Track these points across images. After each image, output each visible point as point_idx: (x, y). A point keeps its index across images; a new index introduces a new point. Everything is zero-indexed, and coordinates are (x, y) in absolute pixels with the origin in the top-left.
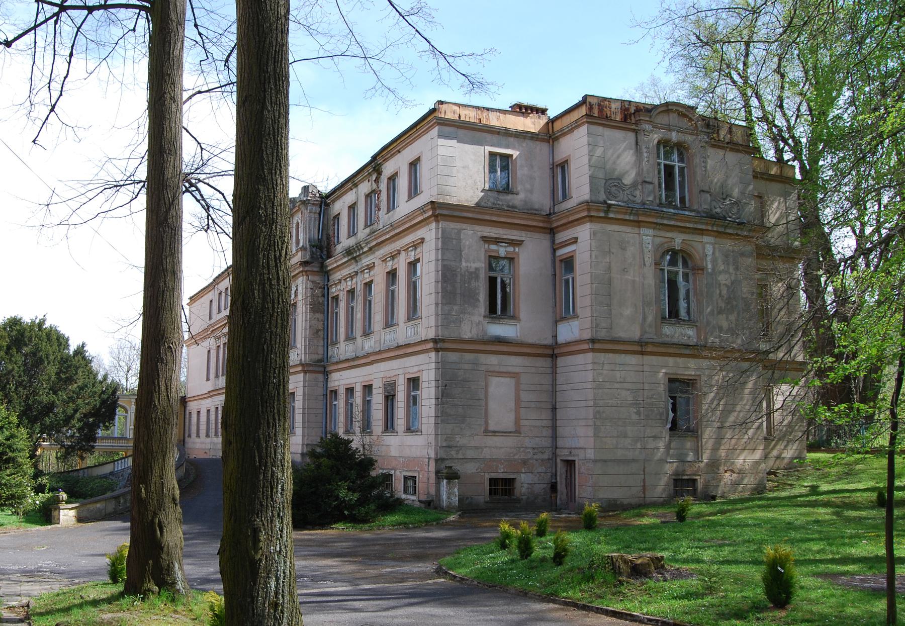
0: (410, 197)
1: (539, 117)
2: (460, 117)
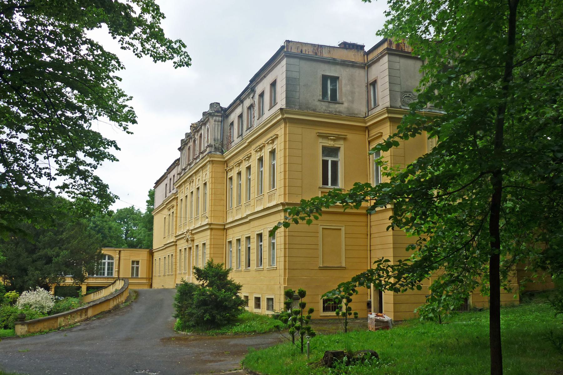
0: (271, 107)
2: (301, 51)
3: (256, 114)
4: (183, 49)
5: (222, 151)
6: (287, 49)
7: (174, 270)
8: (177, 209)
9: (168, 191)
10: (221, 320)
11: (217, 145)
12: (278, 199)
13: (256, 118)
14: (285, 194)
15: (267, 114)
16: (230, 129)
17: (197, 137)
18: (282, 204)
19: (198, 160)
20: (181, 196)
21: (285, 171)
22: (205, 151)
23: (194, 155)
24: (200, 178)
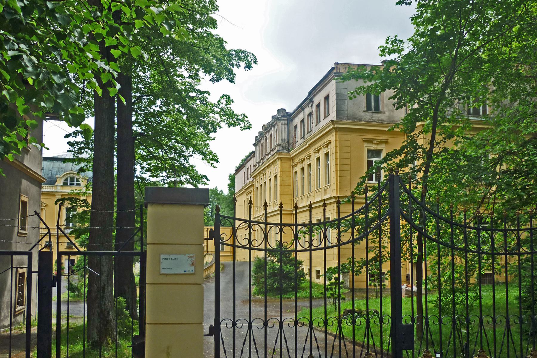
0: (325, 117)
1: (357, 81)
3: (314, 121)
4: (246, 119)
5: (289, 149)
6: (337, 70)
7: (249, 250)
8: (254, 195)
9: (246, 179)
10: (287, 288)
11: (284, 145)
12: (332, 193)
13: (314, 124)
14: (337, 189)
15: (323, 122)
16: (295, 131)
17: (268, 136)
18: (335, 197)
19: (269, 156)
20: (257, 185)
21: (336, 171)
22: (275, 149)
23: (266, 151)
24: (271, 171)
